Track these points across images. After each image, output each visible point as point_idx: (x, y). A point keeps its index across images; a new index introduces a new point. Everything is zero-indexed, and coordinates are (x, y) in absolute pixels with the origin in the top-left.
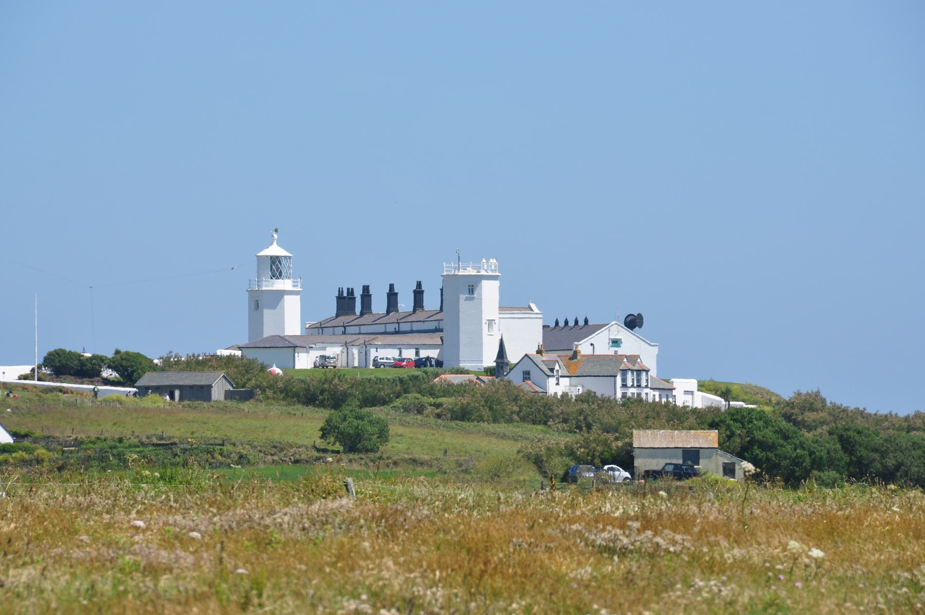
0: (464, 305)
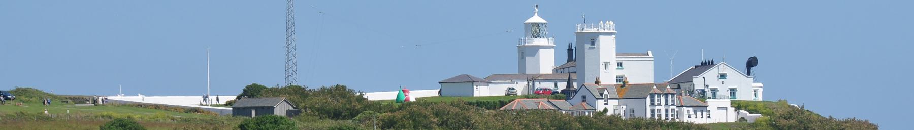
0: (588, 53)
